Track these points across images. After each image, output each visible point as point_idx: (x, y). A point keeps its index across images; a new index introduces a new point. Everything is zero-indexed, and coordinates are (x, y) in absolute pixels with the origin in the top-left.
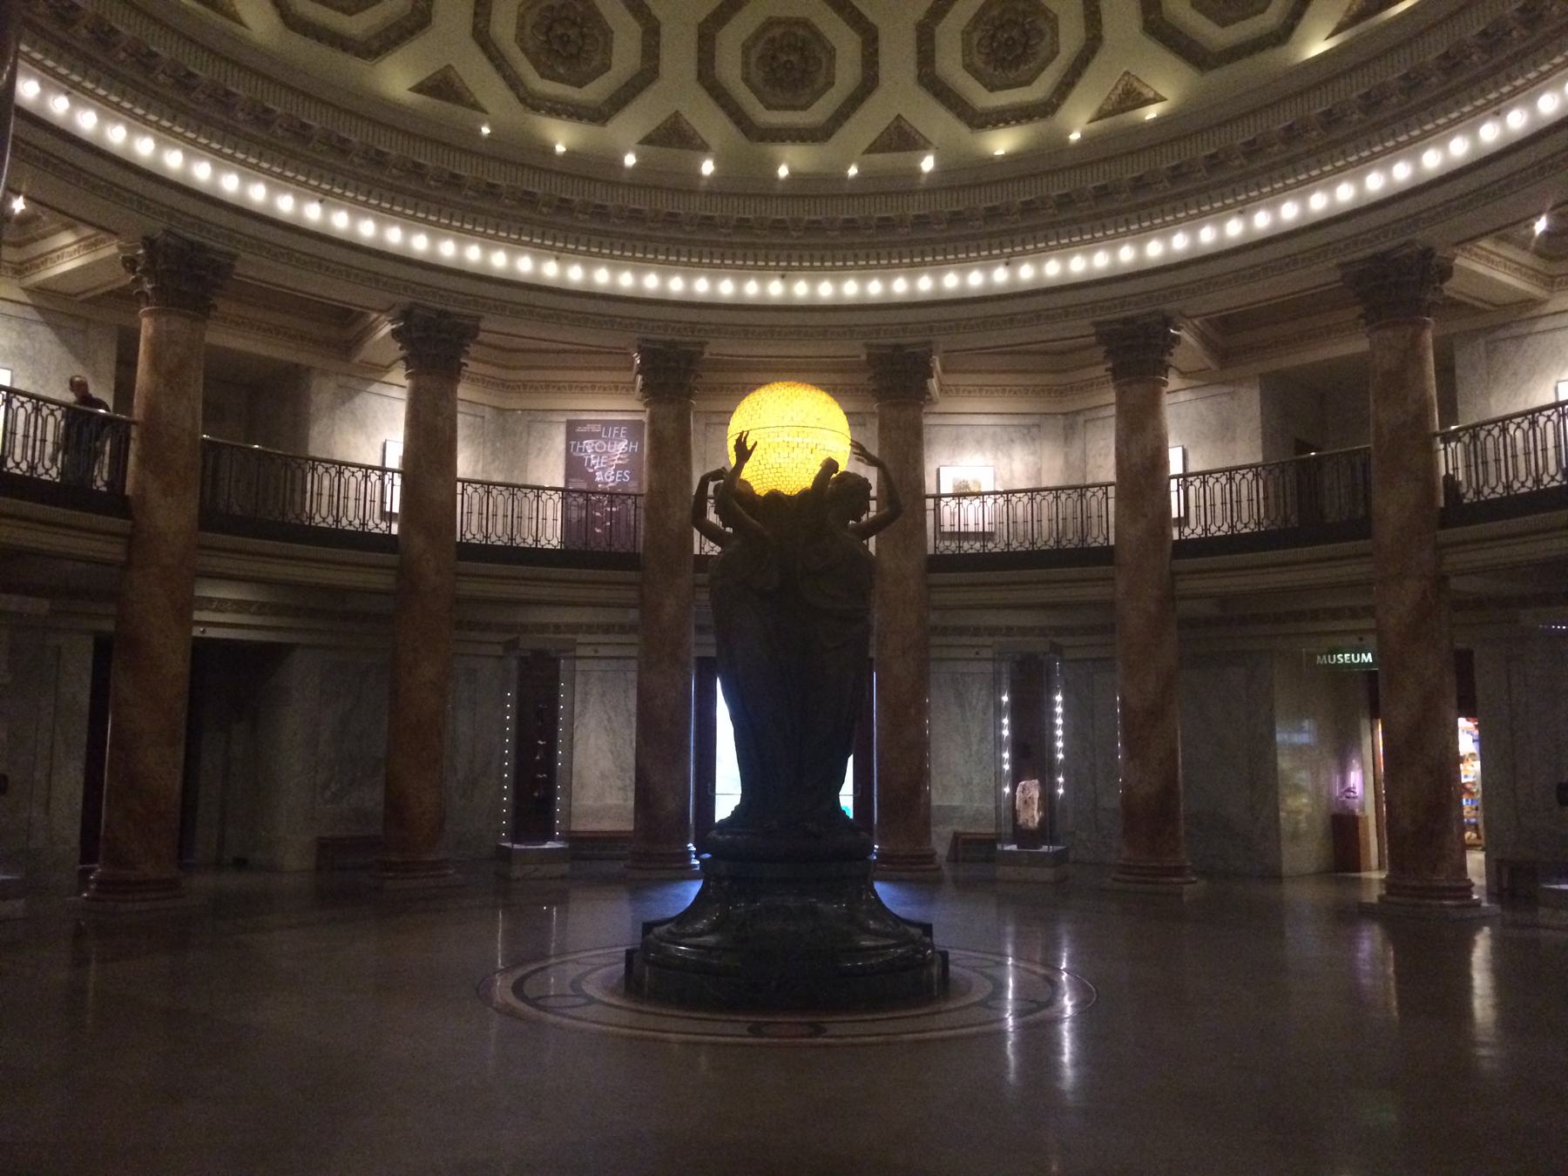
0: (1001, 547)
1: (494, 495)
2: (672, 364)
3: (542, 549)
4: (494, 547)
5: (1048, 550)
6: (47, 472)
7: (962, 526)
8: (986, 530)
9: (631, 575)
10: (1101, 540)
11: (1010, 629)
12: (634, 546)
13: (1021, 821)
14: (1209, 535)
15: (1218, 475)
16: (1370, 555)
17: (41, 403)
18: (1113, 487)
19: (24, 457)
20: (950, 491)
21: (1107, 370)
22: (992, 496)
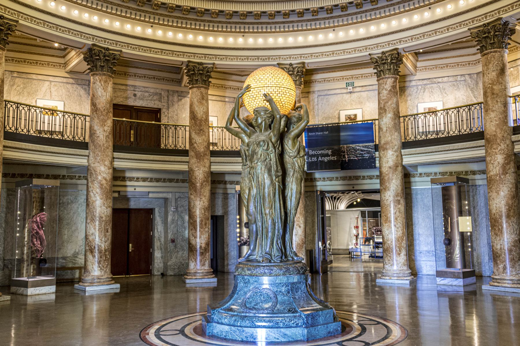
0: (220, 148)
1: (178, 129)
2: (201, 72)
3: (474, 133)
4: (475, 133)
5: (422, 140)
6: (10, 129)
7: (214, 140)
8: (214, 142)
9: (482, 142)
10: (413, 138)
11: (138, 178)
12: (185, 147)
13: (494, 211)
14: (450, 135)
15: (464, 108)
16: (214, 154)
17: (19, 105)
18: (188, 127)
19: (13, 125)
20: (423, 111)
21: (478, 50)
22: (217, 128)
